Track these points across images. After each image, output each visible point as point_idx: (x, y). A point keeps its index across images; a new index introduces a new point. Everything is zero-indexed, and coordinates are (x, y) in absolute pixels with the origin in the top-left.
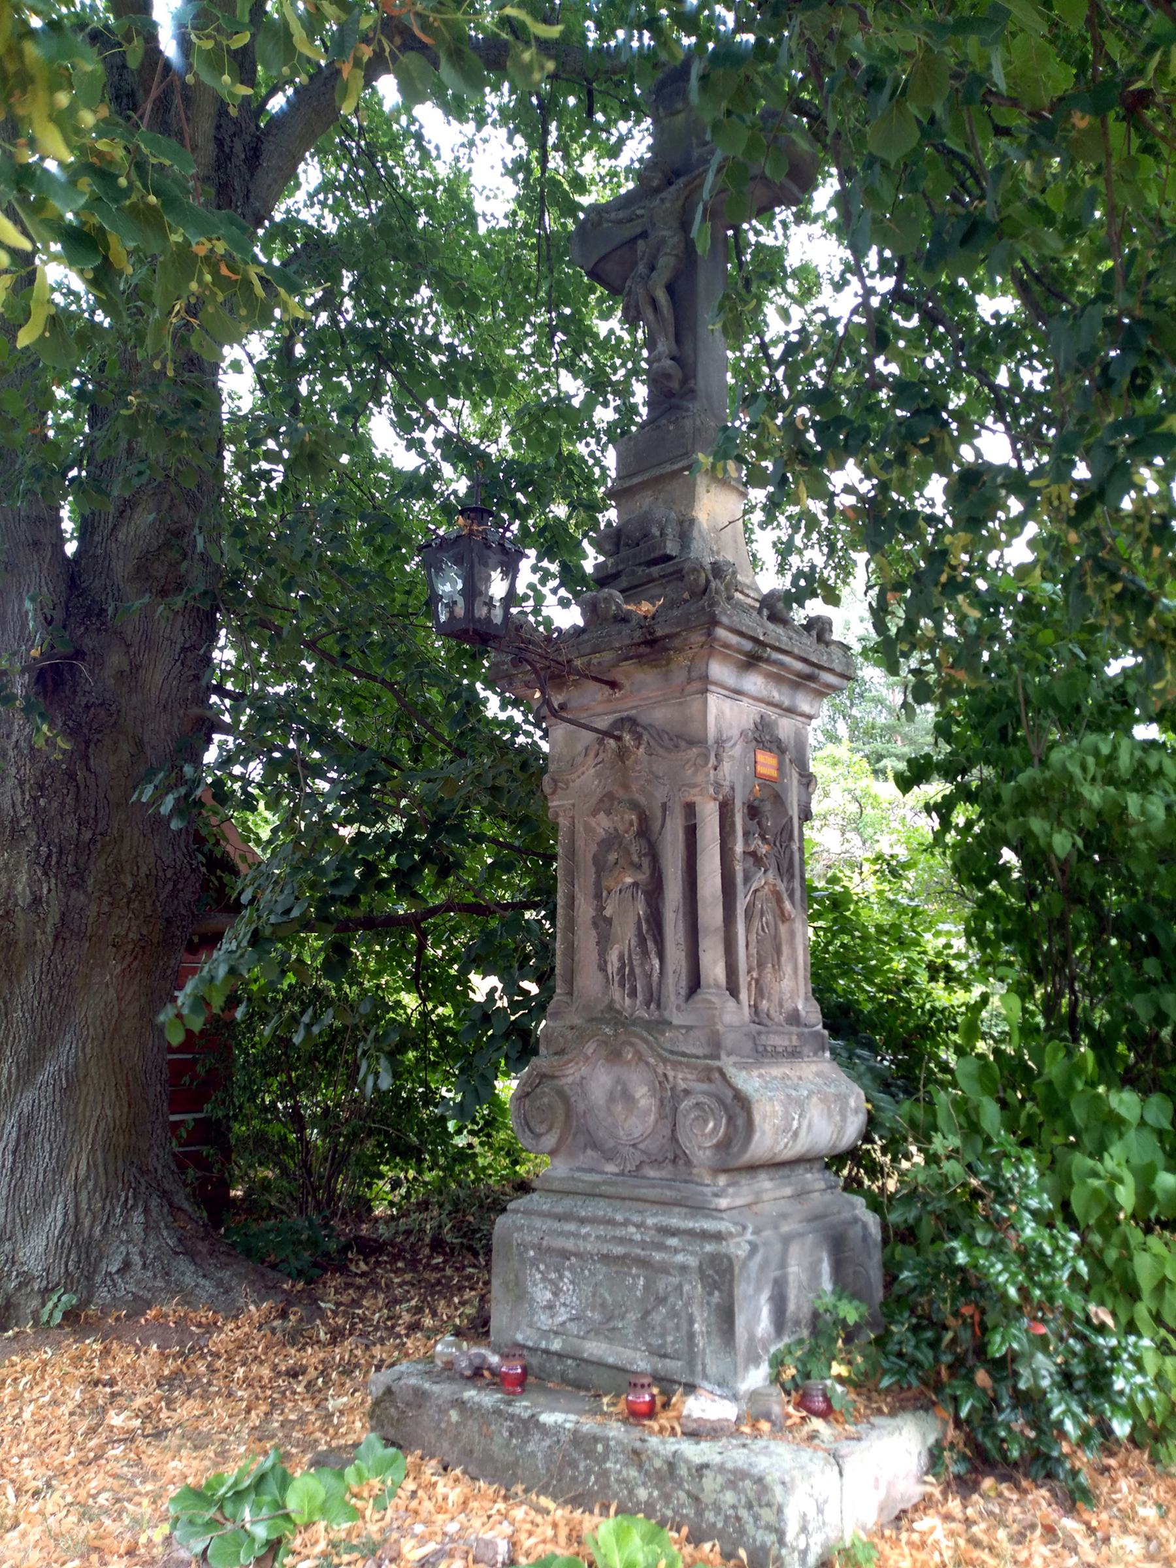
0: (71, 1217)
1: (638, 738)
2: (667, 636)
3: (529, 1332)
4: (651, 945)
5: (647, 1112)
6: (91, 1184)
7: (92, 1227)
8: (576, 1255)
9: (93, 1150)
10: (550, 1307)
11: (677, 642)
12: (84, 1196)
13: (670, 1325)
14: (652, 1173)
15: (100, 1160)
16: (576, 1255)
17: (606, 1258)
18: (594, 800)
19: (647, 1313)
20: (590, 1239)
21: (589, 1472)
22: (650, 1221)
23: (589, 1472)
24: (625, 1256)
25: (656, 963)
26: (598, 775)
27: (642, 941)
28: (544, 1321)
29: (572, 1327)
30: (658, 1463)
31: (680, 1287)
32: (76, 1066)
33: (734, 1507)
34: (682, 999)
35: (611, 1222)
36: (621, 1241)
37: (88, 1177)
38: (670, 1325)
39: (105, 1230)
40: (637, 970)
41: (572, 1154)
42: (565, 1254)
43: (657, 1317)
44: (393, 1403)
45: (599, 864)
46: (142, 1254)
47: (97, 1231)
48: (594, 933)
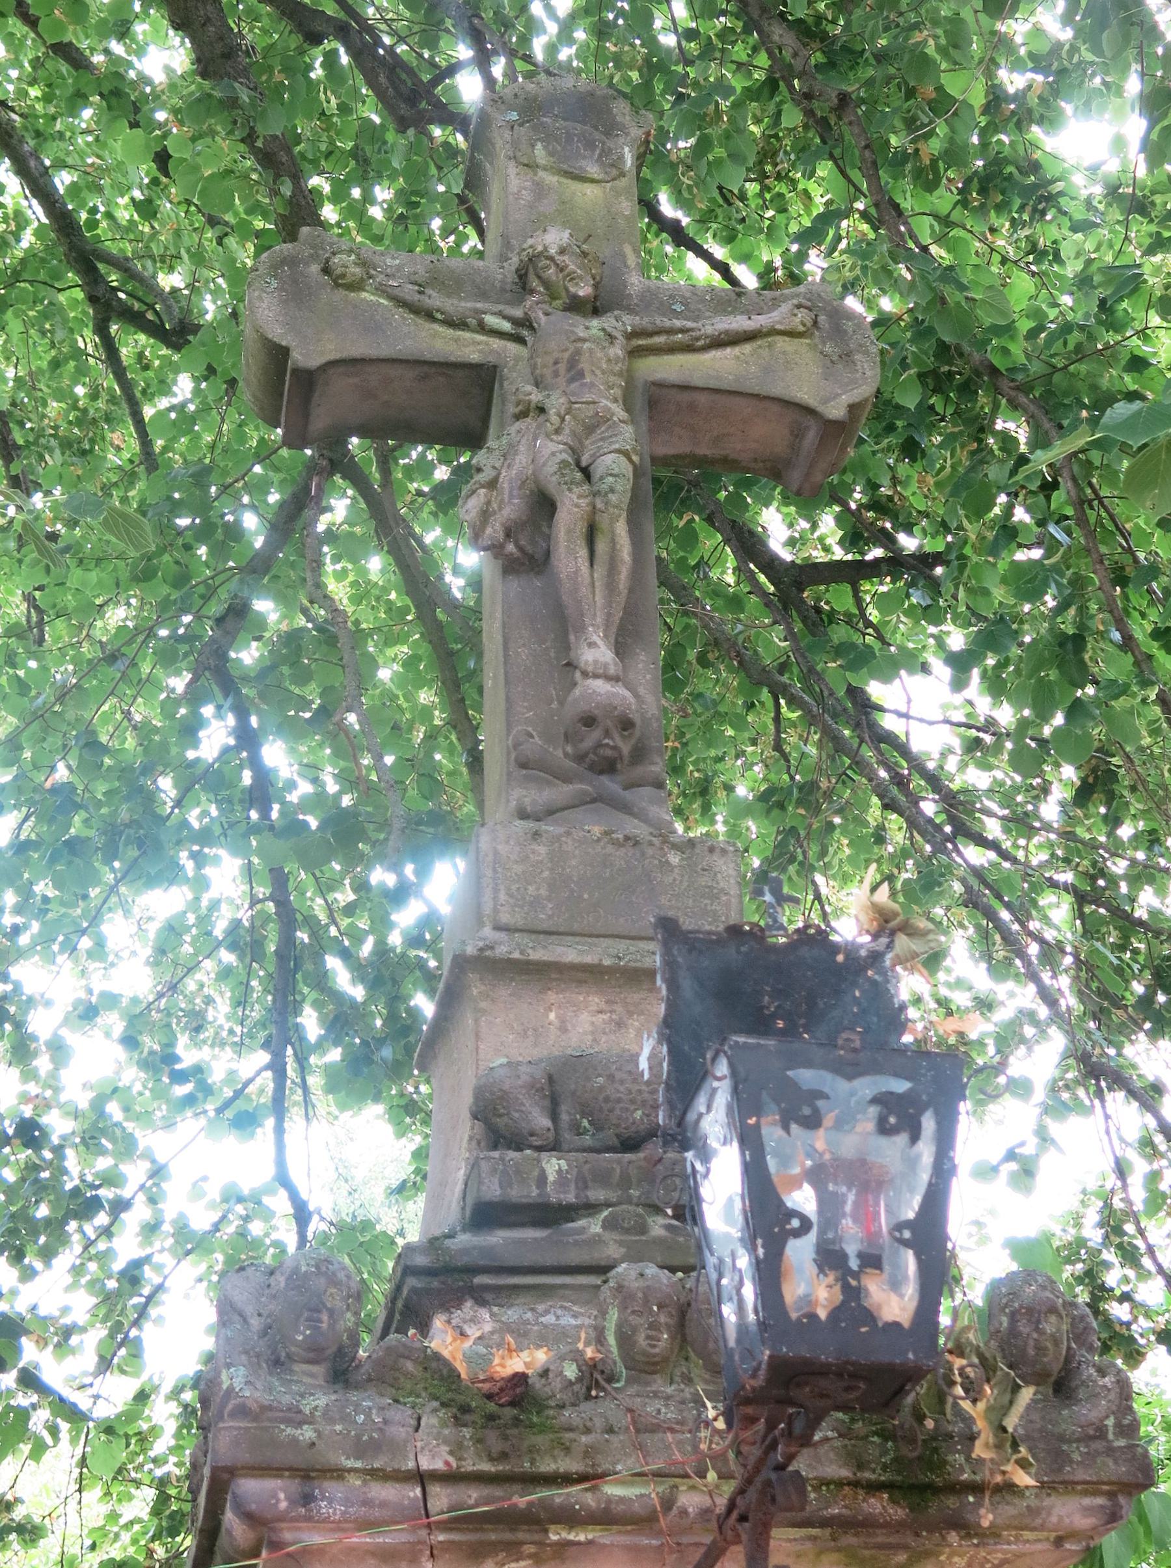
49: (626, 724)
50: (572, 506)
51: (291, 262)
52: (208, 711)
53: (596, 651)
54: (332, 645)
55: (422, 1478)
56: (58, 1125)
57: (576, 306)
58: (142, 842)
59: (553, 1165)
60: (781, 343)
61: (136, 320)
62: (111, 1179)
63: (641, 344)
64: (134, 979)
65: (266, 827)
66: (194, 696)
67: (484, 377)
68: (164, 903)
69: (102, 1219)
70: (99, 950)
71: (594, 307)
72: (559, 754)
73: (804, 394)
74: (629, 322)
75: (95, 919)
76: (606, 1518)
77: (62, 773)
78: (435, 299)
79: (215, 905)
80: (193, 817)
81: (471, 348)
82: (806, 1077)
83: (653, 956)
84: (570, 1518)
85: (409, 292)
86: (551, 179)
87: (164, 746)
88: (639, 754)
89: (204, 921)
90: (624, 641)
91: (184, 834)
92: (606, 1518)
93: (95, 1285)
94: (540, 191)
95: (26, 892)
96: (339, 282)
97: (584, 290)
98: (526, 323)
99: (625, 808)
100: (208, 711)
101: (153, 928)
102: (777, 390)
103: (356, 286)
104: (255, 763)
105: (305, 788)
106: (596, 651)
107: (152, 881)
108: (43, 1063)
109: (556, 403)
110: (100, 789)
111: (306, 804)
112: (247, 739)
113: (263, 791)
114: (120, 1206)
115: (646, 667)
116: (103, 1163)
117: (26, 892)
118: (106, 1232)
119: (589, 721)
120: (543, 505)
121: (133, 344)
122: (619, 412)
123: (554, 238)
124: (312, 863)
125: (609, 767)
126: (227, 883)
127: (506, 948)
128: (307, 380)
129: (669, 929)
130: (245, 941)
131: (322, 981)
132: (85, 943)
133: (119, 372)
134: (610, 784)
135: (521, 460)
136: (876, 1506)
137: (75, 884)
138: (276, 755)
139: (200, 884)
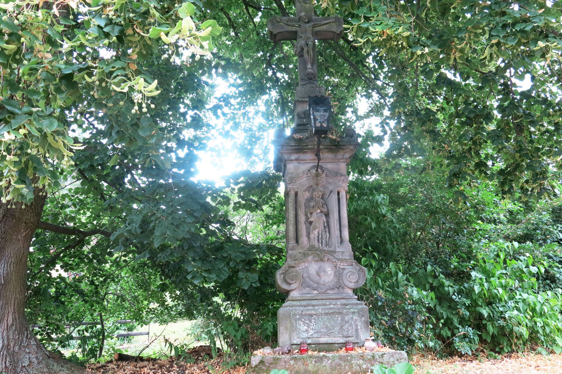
0: (6, 342)
1: (323, 171)
2: (343, 145)
3: (298, 340)
4: (327, 229)
5: (331, 275)
6: (14, 327)
7: (14, 347)
8: (315, 315)
9: (14, 312)
10: (307, 331)
11: (345, 147)
12: (11, 332)
13: (350, 328)
14: (330, 292)
15: (17, 317)
16: (315, 315)
17: (326, 314)
18: (306, 187)
19: (342, 326)
20: (320, 310)
21: (345, 366)
22: (338, 303)
23: (345, 366)
24: (334, 312)
25: (328, 234)
26: (307, 180)
27: (325, 227)
28: (305, 335)
29: (316, 335)
30: (369, 357)
31: (352, 318)
32: (7, 274)
33: (393, 362)
34: (339, 245)
35: (325, 305)
36: (331, 309)
37: (13, 325)
38: (350, 328)
39: (20, 348)
40: (324, 236)
41: (300, 290)
42: (311, 315)
43: (346, 327)
44: (264, 365)
45: (306, 207)
46: (36, 358)
47: (17, 348)
48: (305, 226)
49: (312, 74)
50: (305, 49)
51: (272, 20)
52: (269, 70)
53: (309, 66)
54: (286, 59)
55: (292, 146)
56: (254, 128)
57: (306, 23)
58: (262, 90)
59: (305, 120)
60: (332, 24)
61: (252, 6)
62: (261, 135)
63: (314, 26)
64: (263, 108)
65: (278, 86)
66: (266, 68)
67: (296, 33)
68: (265, 97)
69: (261, 140)
70: (257, 105)
71: (308, 22)
72: (306, 78)
73: (334, 30)
74: (313, 23)
75: (256, 100)
76: (309, 149)
77: (249, 80)
78: (289, 23)
79: (272, 97)
80: (268, 85)
81: (294, 29)
82: (318, 108)
83: (307, 99)
84: (306, 149)
85: (286, 22)
86: (303, 4)
87: (263, 75)
88: (314, 77)
89: (271, 99)
90: (312, 65)
91: (267, 88)
92: (309, 149)
93: (262, 149)
94: (301, 6)
95: (246, 97)
96: (278, 22)
97: (307, 21)
98: (300, 25)
99: (313, 83)
100: (269, 70)
101: (264, 101)
102: (331, 30)
103: (280, 22)
104: (276, 77)
105: (283, 80)
106: (309, 66)
107: (263, 94)
108: (251, 120)
109: (303, 36)
110: (255, 82)
111: (284, 82)
112: (274, 73)
113: (278, 80)
114: (263, 138)
115: (315, 67)
116: (261, 133)
117: (246, 97)
118: (262, 142)
119: (308, 74)
120: (302, 49)
121: (251, 10)
122: (311, 36)
123: (303, 14)
124: (285, 91)
125: (311, 79)
126: (274, 94)
127: (300, 99)
128: (275, 35)
129: (309, 97)
130: (277, 101)
131: (288, 106)
132: (255, 104)
133: (249, 13)
134: (311, 81)
135: (300, 44)
136: (333, 147)
137: (253, 95)
138: (279, 75)
139: (270, 94)
